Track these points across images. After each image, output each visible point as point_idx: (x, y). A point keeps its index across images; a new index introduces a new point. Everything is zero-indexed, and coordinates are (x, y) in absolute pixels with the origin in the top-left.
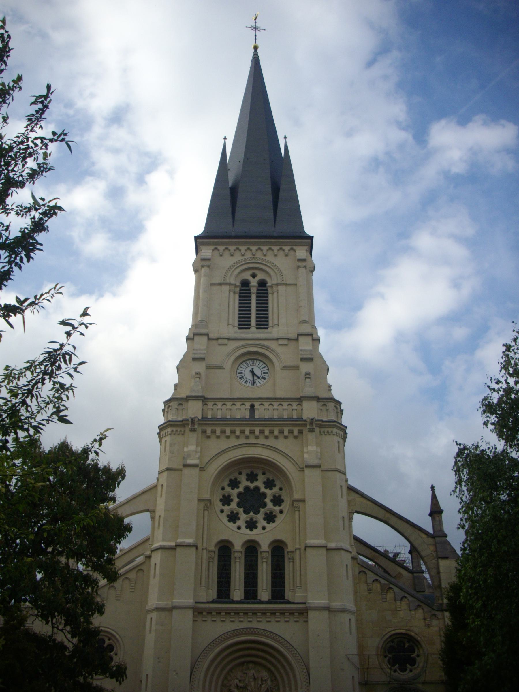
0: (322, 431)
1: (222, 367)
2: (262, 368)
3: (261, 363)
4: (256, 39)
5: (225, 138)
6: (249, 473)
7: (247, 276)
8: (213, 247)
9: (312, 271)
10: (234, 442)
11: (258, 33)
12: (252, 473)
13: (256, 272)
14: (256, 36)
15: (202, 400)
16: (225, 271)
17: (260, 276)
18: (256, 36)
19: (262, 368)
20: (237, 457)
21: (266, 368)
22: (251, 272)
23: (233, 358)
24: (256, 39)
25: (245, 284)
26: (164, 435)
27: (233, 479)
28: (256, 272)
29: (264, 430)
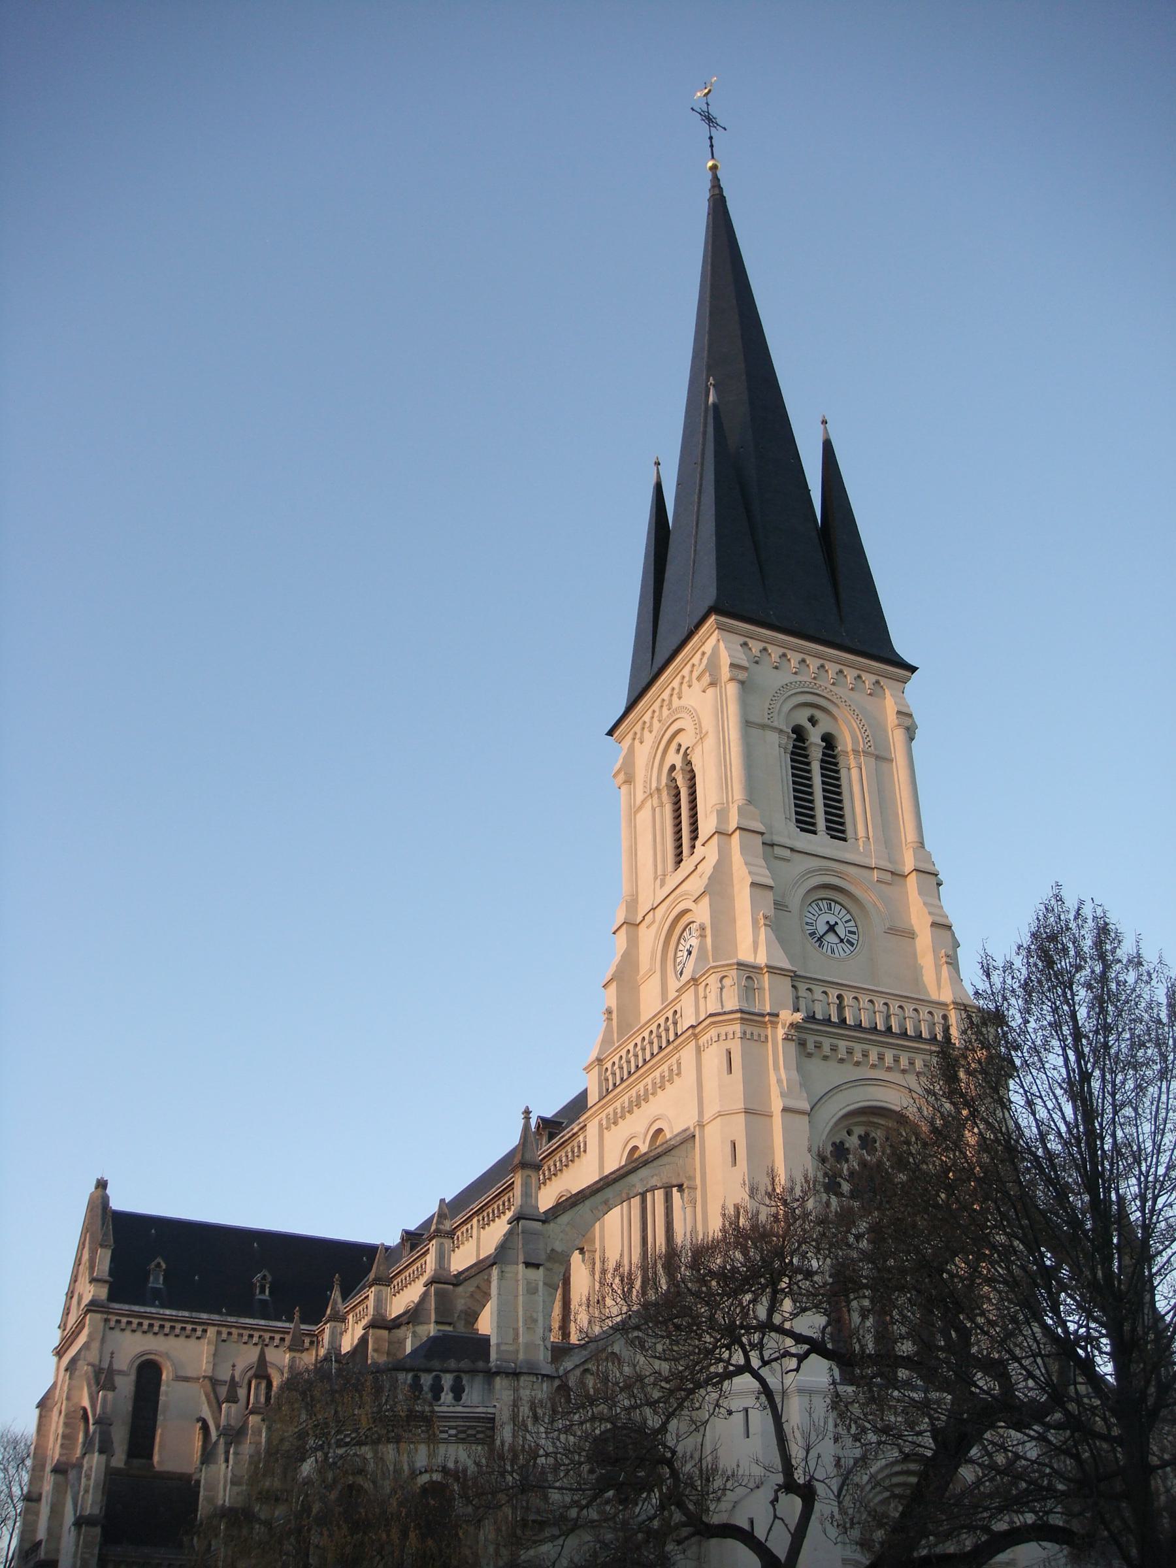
0: (748, 1032)
1: (787, 907)
2: (846, 922)
3: (844, 912)
4: (712, 146)
5: (824, 422)
6: (863, 1133)
7: (802, 718)
8: (742, 639)
9: (913, 740)
10: (850, 1073)
11: (717, 133)
12: (867, 1134)
13: (818, 714)
14: (711, 138)
15: (791, 977)
16: (769, 701)
17: (825, 725)
18: (711, 138)
19: (846, 922)
20: (858, 1102)
21: (852, 923)
22: (808, 712)
23: (802, 891)
24: (712, 146)
25: (799, 733)
26: (706, 1045)
27: (838, 1141)
28: (818, 714)
29: (805, 1041)
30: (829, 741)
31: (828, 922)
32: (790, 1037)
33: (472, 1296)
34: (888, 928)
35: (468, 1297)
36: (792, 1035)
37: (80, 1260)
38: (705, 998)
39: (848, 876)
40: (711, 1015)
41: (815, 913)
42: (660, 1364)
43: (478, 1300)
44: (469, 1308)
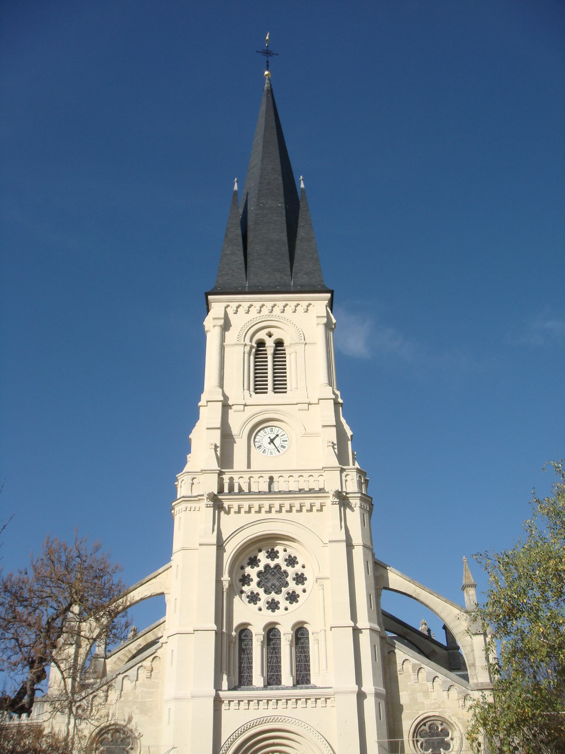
7: (262, 335)
11: (270, 59)
13: (272, 330)
14: (268, 62)
18: (268, 62)
28: (272, 330)
30: (279, 343)
31: (269, 438)
32: (209, 505)
33: (115, 663)
34: (304, 434)
35: (113, 663)
36: (210, 504)
37: (234, 649)
38: (181, 487)
39: (279, 411)
40: (183, 497)
41: (273, 431)
42: (477, 680)
43: (118, 665)
44: (113, 669)
